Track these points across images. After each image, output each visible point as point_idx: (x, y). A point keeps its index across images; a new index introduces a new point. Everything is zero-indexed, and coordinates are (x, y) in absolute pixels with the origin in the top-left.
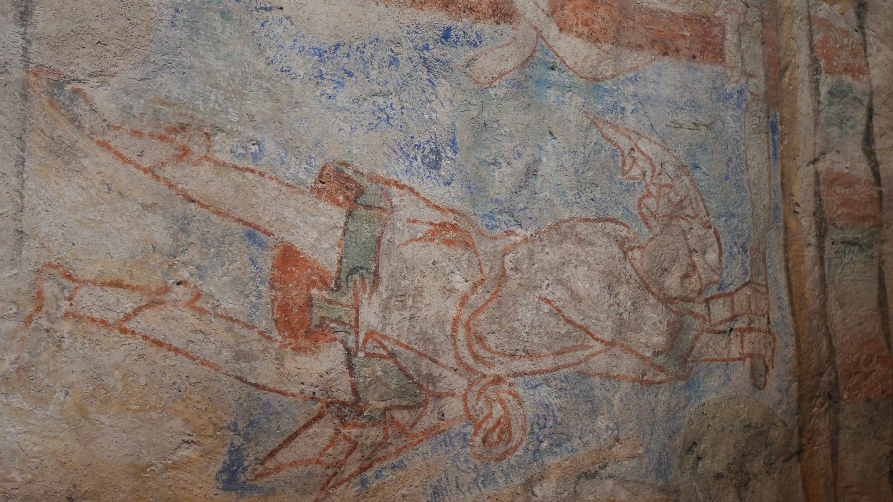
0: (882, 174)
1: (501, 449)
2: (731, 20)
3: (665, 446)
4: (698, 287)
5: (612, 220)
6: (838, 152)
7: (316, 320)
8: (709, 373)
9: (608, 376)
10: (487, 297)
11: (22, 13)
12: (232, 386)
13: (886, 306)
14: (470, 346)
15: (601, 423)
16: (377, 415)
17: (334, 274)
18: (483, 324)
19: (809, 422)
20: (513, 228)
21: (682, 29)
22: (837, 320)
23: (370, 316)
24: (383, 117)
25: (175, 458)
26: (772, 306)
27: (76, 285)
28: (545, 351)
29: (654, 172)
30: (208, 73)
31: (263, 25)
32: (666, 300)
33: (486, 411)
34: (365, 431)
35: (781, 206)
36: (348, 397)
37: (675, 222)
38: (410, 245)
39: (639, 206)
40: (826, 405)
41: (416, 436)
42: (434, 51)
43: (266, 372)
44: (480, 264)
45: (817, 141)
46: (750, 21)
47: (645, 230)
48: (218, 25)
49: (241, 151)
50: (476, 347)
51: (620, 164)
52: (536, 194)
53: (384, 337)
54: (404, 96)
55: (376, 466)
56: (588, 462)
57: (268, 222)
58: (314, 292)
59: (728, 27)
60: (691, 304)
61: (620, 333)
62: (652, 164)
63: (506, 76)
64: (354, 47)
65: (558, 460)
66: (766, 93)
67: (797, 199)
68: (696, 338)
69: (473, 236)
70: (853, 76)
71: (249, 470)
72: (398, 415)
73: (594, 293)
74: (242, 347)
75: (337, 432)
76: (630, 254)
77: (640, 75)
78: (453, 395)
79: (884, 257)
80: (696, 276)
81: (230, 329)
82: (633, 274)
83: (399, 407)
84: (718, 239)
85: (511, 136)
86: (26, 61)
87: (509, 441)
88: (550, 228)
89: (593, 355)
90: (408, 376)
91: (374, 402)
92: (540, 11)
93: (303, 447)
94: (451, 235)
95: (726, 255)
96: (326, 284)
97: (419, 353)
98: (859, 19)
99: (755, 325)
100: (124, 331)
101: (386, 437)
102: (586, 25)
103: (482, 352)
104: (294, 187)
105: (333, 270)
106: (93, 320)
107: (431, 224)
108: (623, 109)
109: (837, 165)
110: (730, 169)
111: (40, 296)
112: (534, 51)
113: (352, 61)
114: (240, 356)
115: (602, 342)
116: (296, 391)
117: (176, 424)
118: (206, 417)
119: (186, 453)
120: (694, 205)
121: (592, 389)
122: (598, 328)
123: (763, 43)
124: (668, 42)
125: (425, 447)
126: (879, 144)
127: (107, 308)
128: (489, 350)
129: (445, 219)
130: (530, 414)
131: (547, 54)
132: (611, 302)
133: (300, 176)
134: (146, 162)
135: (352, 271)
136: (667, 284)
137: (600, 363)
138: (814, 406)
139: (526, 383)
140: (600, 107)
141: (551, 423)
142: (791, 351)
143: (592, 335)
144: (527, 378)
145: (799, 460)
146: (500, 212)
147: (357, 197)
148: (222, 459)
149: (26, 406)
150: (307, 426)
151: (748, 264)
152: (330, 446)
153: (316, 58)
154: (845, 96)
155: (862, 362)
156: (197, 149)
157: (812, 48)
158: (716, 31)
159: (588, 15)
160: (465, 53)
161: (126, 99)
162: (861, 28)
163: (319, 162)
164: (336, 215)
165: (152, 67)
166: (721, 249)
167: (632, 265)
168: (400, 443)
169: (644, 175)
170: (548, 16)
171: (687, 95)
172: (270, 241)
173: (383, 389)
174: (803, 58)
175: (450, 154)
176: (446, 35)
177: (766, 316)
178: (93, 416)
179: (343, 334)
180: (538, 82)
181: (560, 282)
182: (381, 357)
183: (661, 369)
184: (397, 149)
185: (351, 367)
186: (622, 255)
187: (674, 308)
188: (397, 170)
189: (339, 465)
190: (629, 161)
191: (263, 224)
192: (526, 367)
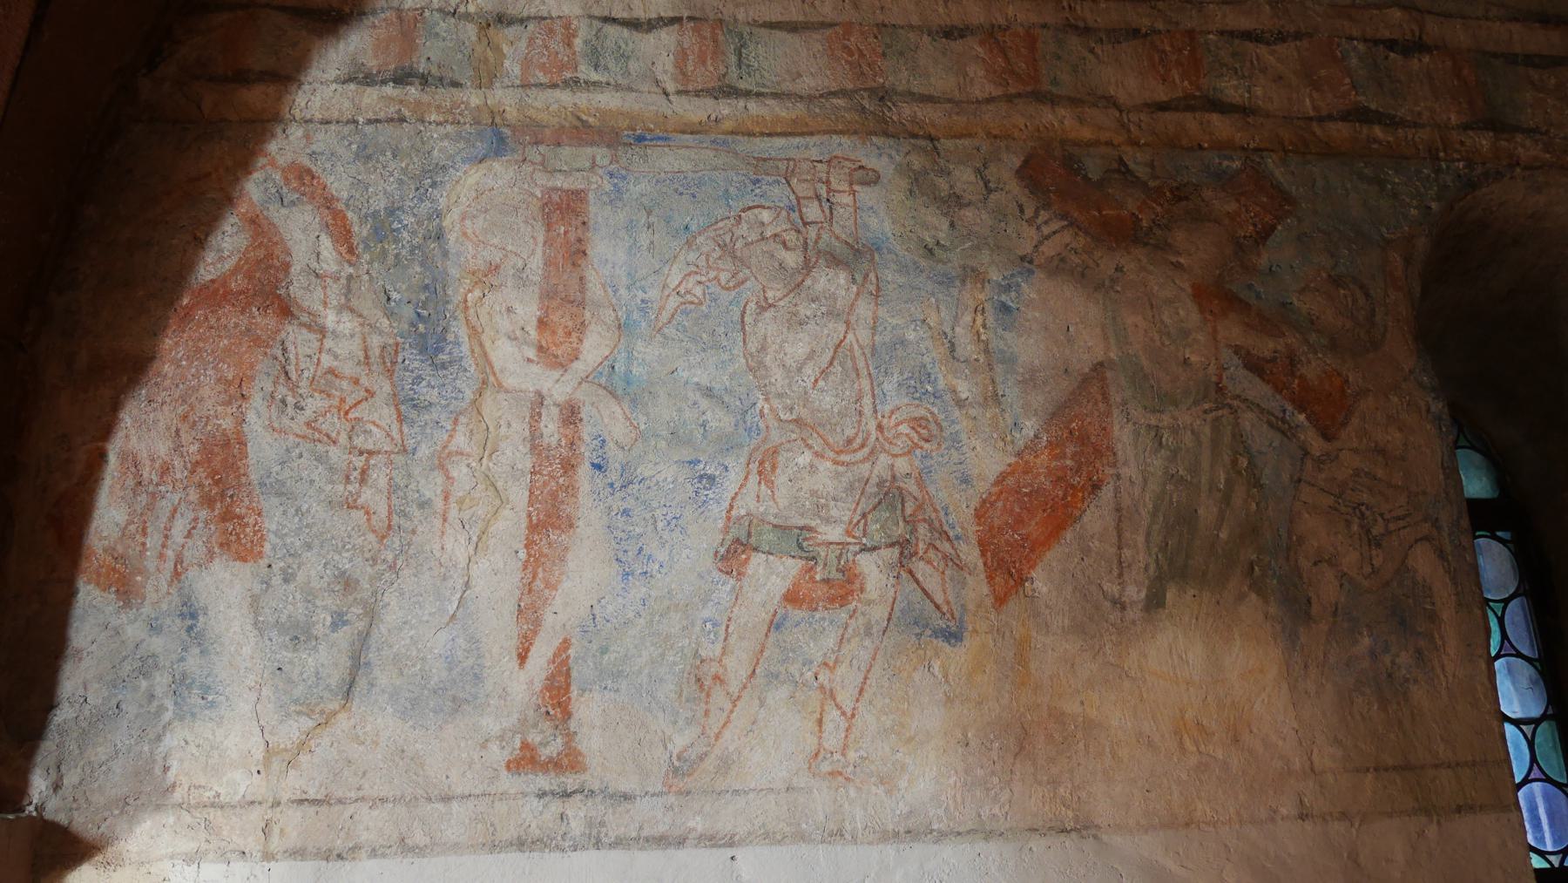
0: (671, 14)
1: (933, 426)
2: (542, 179)
3: (929, 278)
4: (793, 232)
5: (743, 317)
6: (653, 63)
7: (839, 576)
8: (866, 226)
9: (874, 328)
10: (815, 435)
11: (625, 799)
12: (889, 638)
13: (796, 22)
14: (855, 451)
15: (911, 336)
16: (909, 528)
17: (804, 562)
18: (837, 439)
19: (904, 125)
20: (758, 412)
21: (559, 234)
22: (813, 84)
23: (834, 533)
24: (674, 522)
25: (940, 676)
26: (806, 156)
27: (822, 750)
28: (856, 386)
29: (696, 273)
30: (653, 663)
31: (608, 621)
32: (807, 267)
33: (905, 438)
34: (921, 537)
35: (713, 137)
36: (896, 550)
37: (739, 254)
38: (778, 500)
39: (728, 289)
40: (889, 104)
41: (923, 496)
42: (614, 478)
43: (879, 613)
44: (789, 441)
45: (646, 89)
46: (539, 158)
47: (748, 284)
48: (613, 656)
49: (712, 636)
50: (855, 445)
51: (693, 307)
52: (726, 389)
53: (850, 523)
54: (655, 504)
55: (946, 528)
56: (942, 350)
57: (767, 613)
58: (818, 577)
59: (550, 184)
60: (808, 241)
61: (838, 315)
62: (689, 275)
63: (628, 413)
64: (617, 547)
65: (940, 376)
66: (608, 146)
67: (705, 119)
68: (837, 238)
69: (767, 447)
70: (574, 36)
71: (949, 623)
72: (909, 511)
73: (807, 339)
74: (862, 632)
75: (922, 558)
76: (770, 301)
77: (609, 281)
78: (893, 465)
79: (750, 20)
80: (784, 234)
81: (849, 641)
82: (787, 299)
83: (903, 510)
84: (750, 208)
85: (680, 410)
86: (660, 794)
87: (927, 420)
88: (755, 377)
89: (857, 341)
90: (880, 503)
91: (900, 530)
92: (562, 379)
93: (932, 583)
94: (767, 465)
95: (763, 202)
96: (812, 568)
97: (862, 494)
98: (513, 23)
99: (824, 176)
100: (853, 716)
101: (925, 520)
102: (570, 333)
103: (859, 441)
104: (737, 595)
105: (801, 563)
106: (846, 737)
107: (760, 483)
108: (643, 301)
109: (666, 68)
110: (685, 192)
111: (831, 774)
112: (600, 385)
113: (630, 548)
114: (868, 633)
115: (846, 332)
116: (893, 590)
117: (917, 676)
118: (912, 656)
119: (937, 669)
120: (722, 232)
121: (884, 344)
122: (835, 335)
123: (559, 144)
124: (573, 249)
125: (932, 489)
126: (639, 13)
127: (837, 728)
128: (857, 434)
129: (755, 471)
130: (906, 401)
131: (601, 373)
132: (813, 322)
133: (728, 589)
134: (727, 706)
135: (801, 548)
136: (793, 265)
137: (864, 335)
138: (891, 118)
139: (882, 403)
140: (644, 324)
141: (913, 382)
142: (845, 140)
143: (842, 341)
144: (877, 402)
145: (938, 140)
146: (745, 422)
147: (742, 544)
148: (941, 643)
149: (906, 777)
150: (917, 581)
151: (770, 179)
152: (932, 564)
153: (630, 577)
154: (596, 48)
155: (850, 59)
156: (714, 668)
157: (554, 86)
158: (556, 198)
159: (560, 332)
160: (611, 450)
161: (681, 723)
162: (522, 21)
163: (716, 575)
164: (757, 559)
165: (653, 704)
166: (758, 207)
167: (780, 299)
168: (929, 510)
169: (700, 282)
170: (566, 371)
171: (622, 233)
172: (781, 612)
173: (889, 522)
174: (565, 97)
175: (702, 466)
176: (598, 467)
177: (815, 164)
178: (912, 733)
179: (849, 554)
180: (628, 383)
181: (799, 370)
182: (866, 524)
183: (866, 276)
184: (700, 510)
185: (874, 549)
186: (772, 309)
187: (814, 259)
188: (717, 511)
189: (945, 557)
190: (689, 297)
191: (768, 618)
192: (869, 402)
